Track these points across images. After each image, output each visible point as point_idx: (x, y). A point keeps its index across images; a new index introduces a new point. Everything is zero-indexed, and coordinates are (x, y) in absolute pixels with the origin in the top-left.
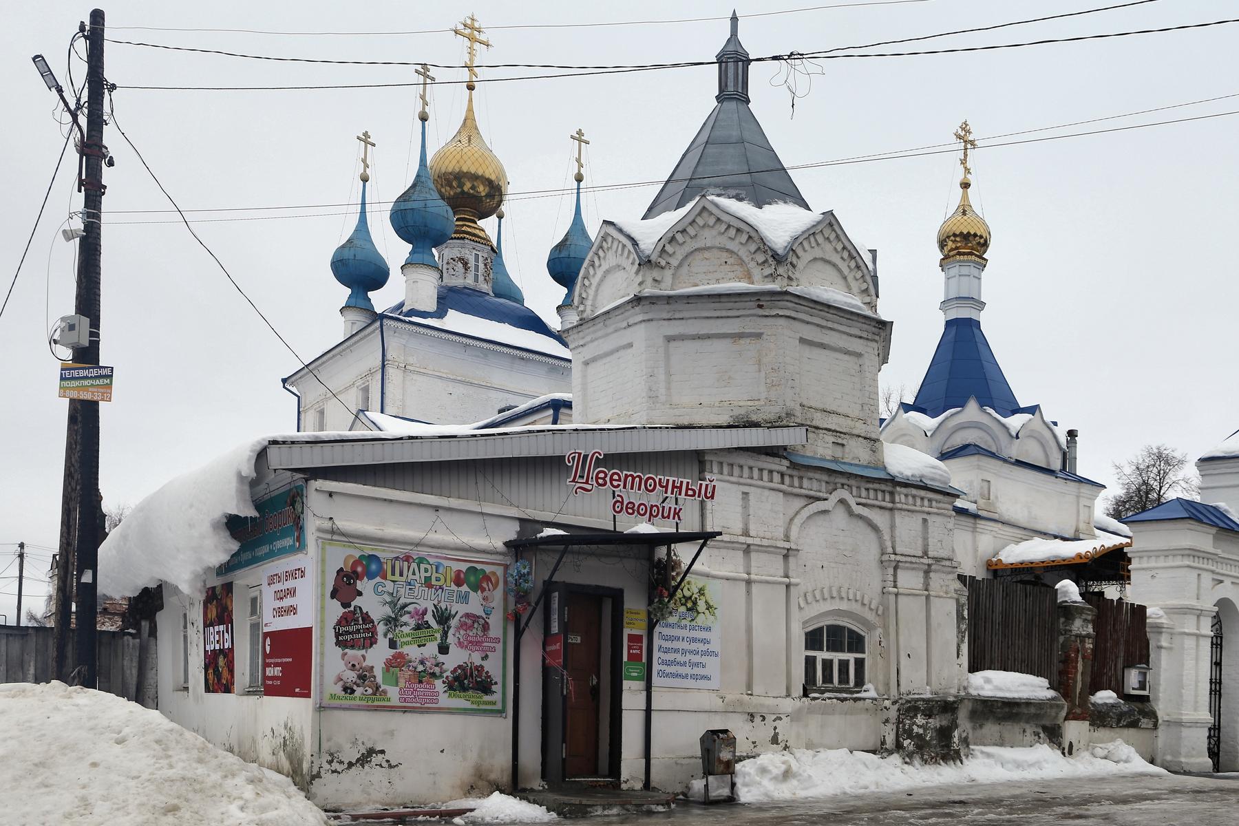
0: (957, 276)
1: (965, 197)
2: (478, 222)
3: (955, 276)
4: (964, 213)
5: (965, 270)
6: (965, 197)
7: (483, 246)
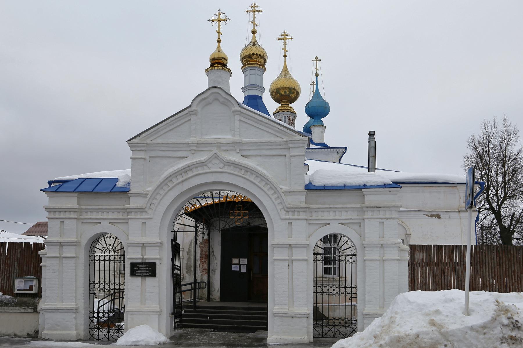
0: (249, 74)
1: (254, 37)
2: (290, 105)
3: (248, 75)
4: (254, 44)
5: (253, 72)
6: (254, 37)
7: (287, 113)
